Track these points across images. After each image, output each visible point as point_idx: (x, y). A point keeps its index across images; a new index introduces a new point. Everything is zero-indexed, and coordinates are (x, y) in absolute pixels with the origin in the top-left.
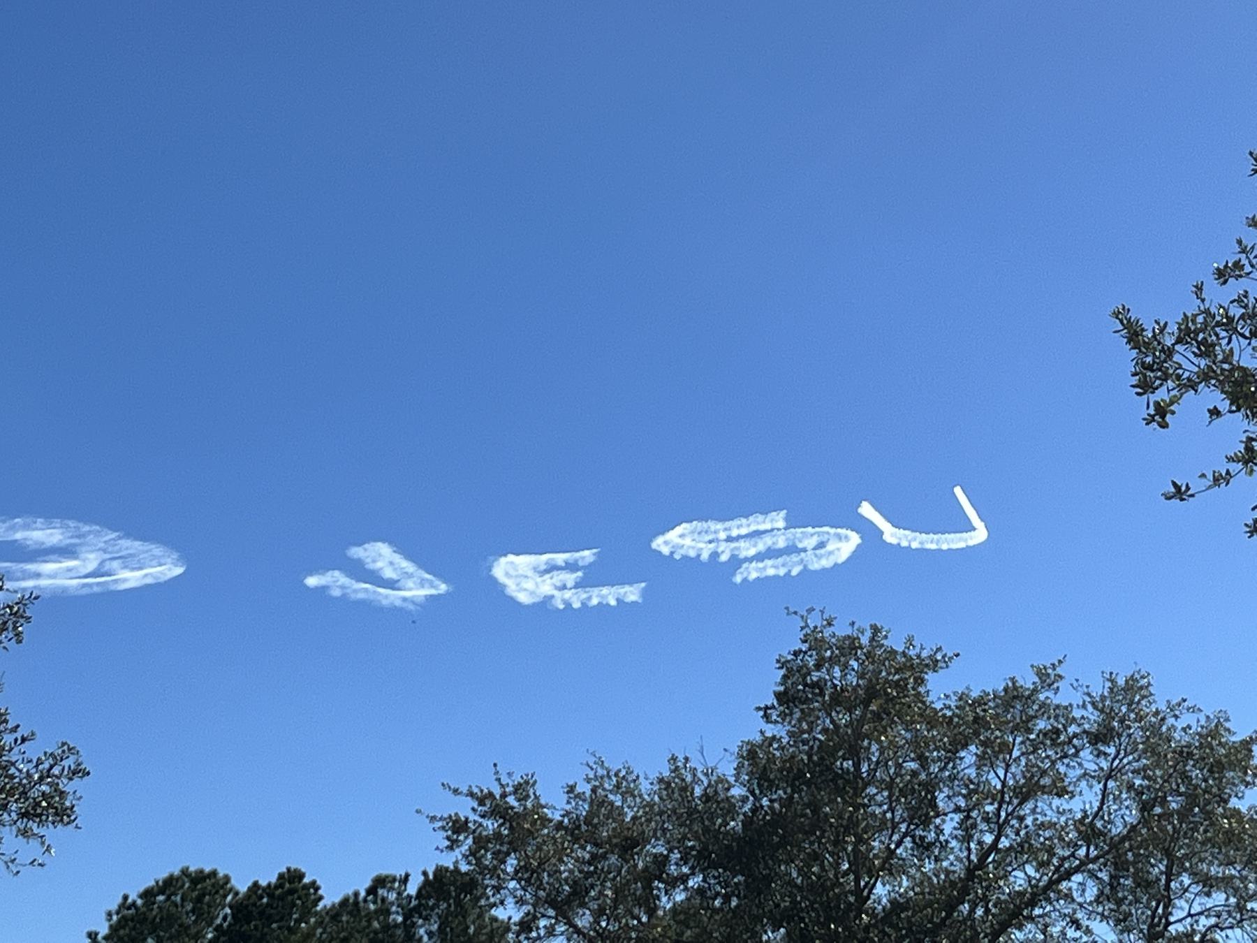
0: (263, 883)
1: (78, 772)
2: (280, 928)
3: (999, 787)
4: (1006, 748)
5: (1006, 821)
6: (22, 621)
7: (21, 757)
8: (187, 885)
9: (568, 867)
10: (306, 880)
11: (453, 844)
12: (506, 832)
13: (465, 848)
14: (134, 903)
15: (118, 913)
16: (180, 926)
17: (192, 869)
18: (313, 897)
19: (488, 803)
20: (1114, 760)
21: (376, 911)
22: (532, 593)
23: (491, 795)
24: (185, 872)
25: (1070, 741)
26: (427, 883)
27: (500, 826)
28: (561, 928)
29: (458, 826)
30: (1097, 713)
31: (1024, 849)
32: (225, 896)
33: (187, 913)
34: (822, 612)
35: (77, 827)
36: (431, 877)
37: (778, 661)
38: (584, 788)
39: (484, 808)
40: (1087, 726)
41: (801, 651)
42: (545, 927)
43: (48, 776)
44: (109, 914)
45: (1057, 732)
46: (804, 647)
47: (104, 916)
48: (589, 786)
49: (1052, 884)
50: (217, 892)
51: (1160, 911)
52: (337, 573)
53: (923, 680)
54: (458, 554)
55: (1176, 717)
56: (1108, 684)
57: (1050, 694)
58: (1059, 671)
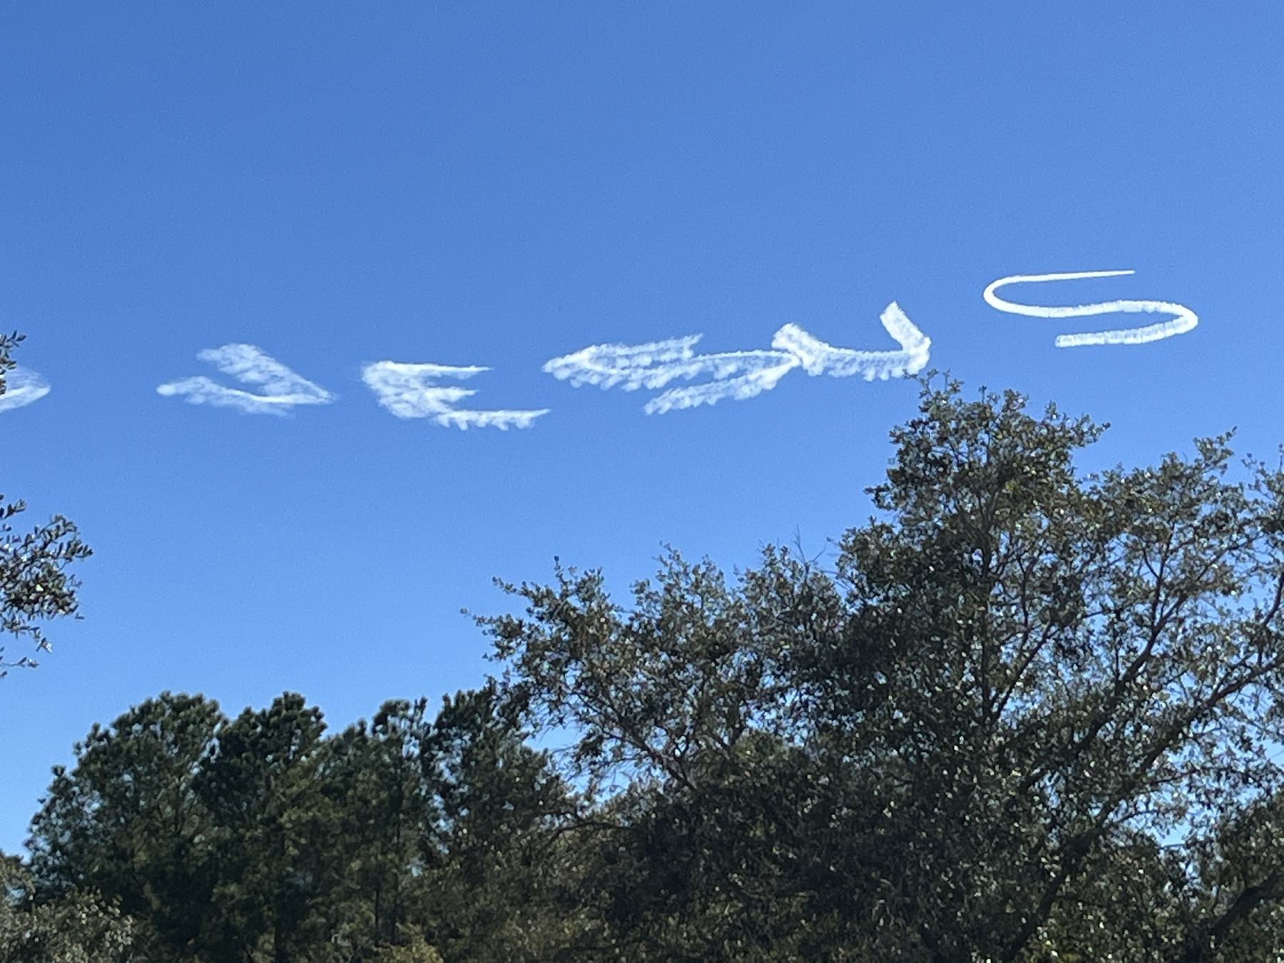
0: (257, 711)
1: (74, 550)
2: (275, 760)
3: (1153, 584)
4: (1164, 536)
8: (168, 712)
9: (638, 679)
10: (307, 707)
11: (504, 651)
13: (517, 657)
14: (106, 735)
15: (87, 746)
16: (160, 758)
18: (314, 726)
19: (546, 601)
21: (386, 743)
23: (549, 593)
24: (165, 698)
26: (448, 711)
27: (560, 630)
28: (629, 751)
29: (510, 631)
31: (1182, 657)
32: (212, 725)
33: (169, 745)
34: (947, 376)
35: (77, 617)
36: (453, 704)
37: (892, 434)
38: (657, 587)
39: (540, 609)
40: (1260, 511)
41: (921, 422)
42: (612, 750)
43: (42, 556)
44: (78, 747)
45: (1226, 518)
48: (662, 585)
49: (1217, 696)
53: (1066, 456)
57: (1216, 472)
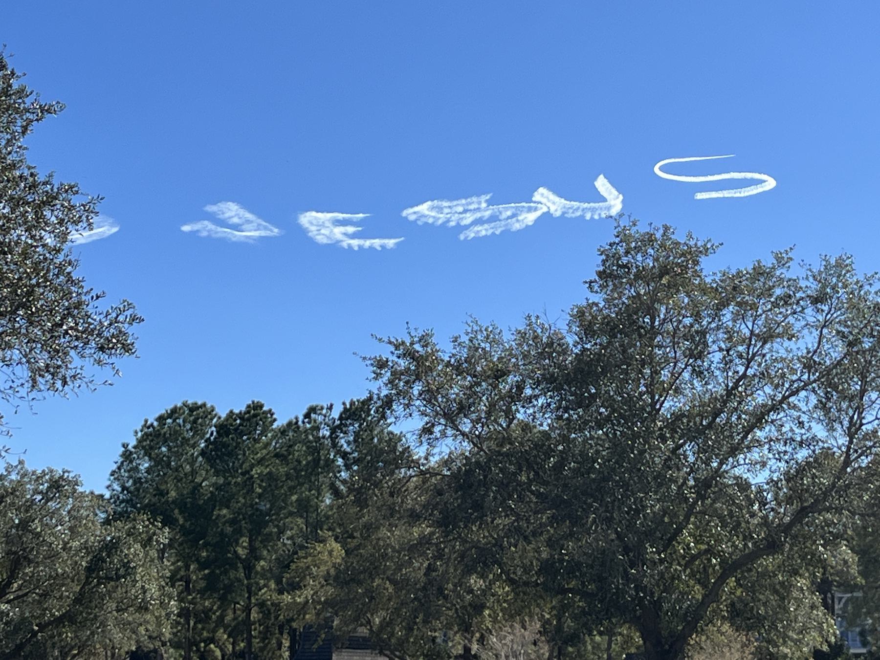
0: (237, 411)
2: (248, 439)
3: (748, 334)
5: (754, 355)
6: (92, 215)
7: (94, 310)
9: (455, 391)
10: (265, 409)
11: (378, 376)
12: (413, 368)
14: (152, 425)
15: (141, 431)
17: (190, 402)
20: (827, 315)
22: (328, 237)
23: (403, 343)
25: (798, 303)
29: (381, 364)
30: (815, 283)
32: (212, 419)
33: (187, 431)
34: (629, 216)
36: (348, 406)
37: (599, 250)
38: (465, 339)
40: (809, 292)
41: (615, 243)
44: (136, 432)
45: (790, 296)
46: (617, 240)
47: (133, 433)
48: (468, 338)
50: (206, 417)
51: (856, 417)
52: (206, 222)
53: (698, 262)
54: (281, 211)
55: (870, 284)
56: (824, 263)
57: (784, 271)
58: (790, 255)
